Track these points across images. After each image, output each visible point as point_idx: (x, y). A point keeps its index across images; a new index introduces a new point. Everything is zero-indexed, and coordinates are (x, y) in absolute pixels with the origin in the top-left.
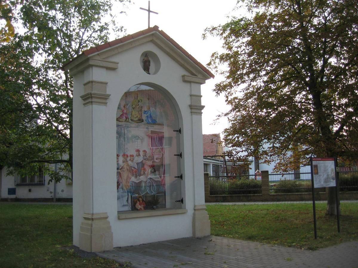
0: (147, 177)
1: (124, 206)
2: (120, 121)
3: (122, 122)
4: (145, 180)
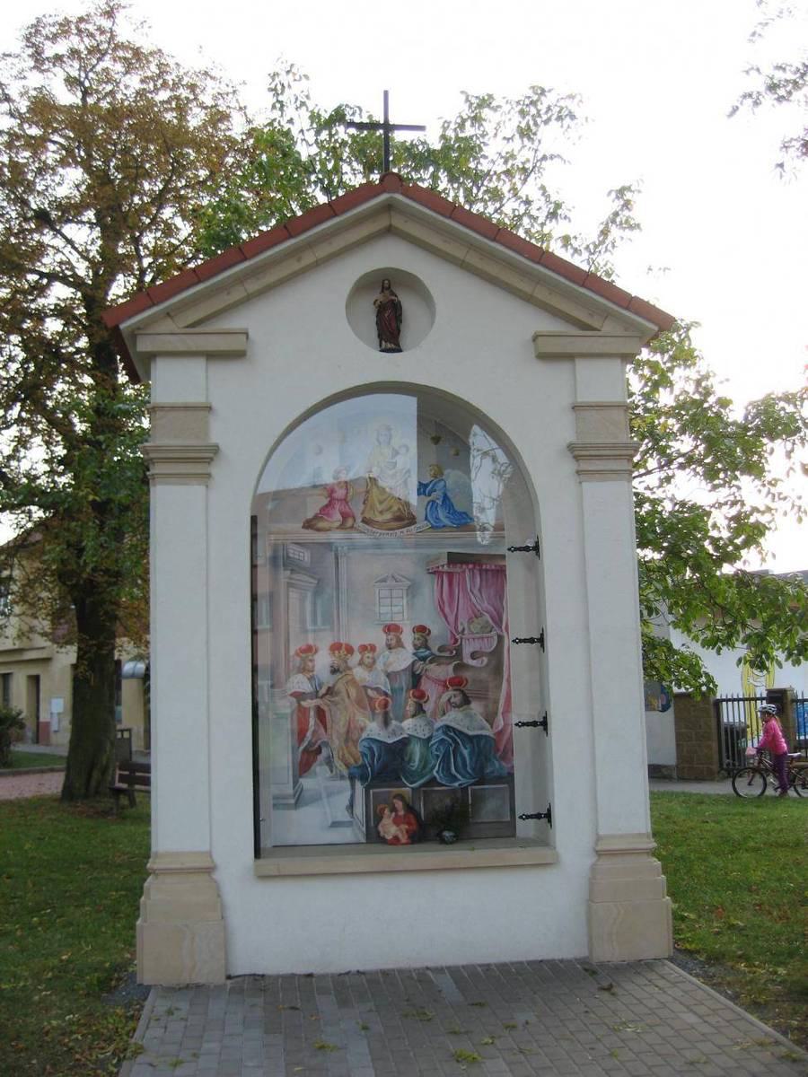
0: (430, 724)
1: (335, 825)
2: (319, 530)
3: (329, 530)
4: (423, 733)
